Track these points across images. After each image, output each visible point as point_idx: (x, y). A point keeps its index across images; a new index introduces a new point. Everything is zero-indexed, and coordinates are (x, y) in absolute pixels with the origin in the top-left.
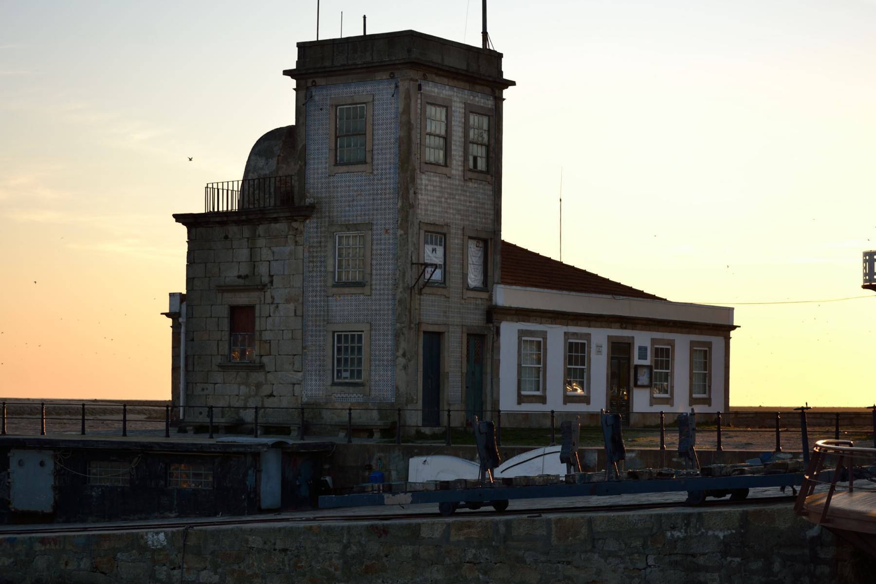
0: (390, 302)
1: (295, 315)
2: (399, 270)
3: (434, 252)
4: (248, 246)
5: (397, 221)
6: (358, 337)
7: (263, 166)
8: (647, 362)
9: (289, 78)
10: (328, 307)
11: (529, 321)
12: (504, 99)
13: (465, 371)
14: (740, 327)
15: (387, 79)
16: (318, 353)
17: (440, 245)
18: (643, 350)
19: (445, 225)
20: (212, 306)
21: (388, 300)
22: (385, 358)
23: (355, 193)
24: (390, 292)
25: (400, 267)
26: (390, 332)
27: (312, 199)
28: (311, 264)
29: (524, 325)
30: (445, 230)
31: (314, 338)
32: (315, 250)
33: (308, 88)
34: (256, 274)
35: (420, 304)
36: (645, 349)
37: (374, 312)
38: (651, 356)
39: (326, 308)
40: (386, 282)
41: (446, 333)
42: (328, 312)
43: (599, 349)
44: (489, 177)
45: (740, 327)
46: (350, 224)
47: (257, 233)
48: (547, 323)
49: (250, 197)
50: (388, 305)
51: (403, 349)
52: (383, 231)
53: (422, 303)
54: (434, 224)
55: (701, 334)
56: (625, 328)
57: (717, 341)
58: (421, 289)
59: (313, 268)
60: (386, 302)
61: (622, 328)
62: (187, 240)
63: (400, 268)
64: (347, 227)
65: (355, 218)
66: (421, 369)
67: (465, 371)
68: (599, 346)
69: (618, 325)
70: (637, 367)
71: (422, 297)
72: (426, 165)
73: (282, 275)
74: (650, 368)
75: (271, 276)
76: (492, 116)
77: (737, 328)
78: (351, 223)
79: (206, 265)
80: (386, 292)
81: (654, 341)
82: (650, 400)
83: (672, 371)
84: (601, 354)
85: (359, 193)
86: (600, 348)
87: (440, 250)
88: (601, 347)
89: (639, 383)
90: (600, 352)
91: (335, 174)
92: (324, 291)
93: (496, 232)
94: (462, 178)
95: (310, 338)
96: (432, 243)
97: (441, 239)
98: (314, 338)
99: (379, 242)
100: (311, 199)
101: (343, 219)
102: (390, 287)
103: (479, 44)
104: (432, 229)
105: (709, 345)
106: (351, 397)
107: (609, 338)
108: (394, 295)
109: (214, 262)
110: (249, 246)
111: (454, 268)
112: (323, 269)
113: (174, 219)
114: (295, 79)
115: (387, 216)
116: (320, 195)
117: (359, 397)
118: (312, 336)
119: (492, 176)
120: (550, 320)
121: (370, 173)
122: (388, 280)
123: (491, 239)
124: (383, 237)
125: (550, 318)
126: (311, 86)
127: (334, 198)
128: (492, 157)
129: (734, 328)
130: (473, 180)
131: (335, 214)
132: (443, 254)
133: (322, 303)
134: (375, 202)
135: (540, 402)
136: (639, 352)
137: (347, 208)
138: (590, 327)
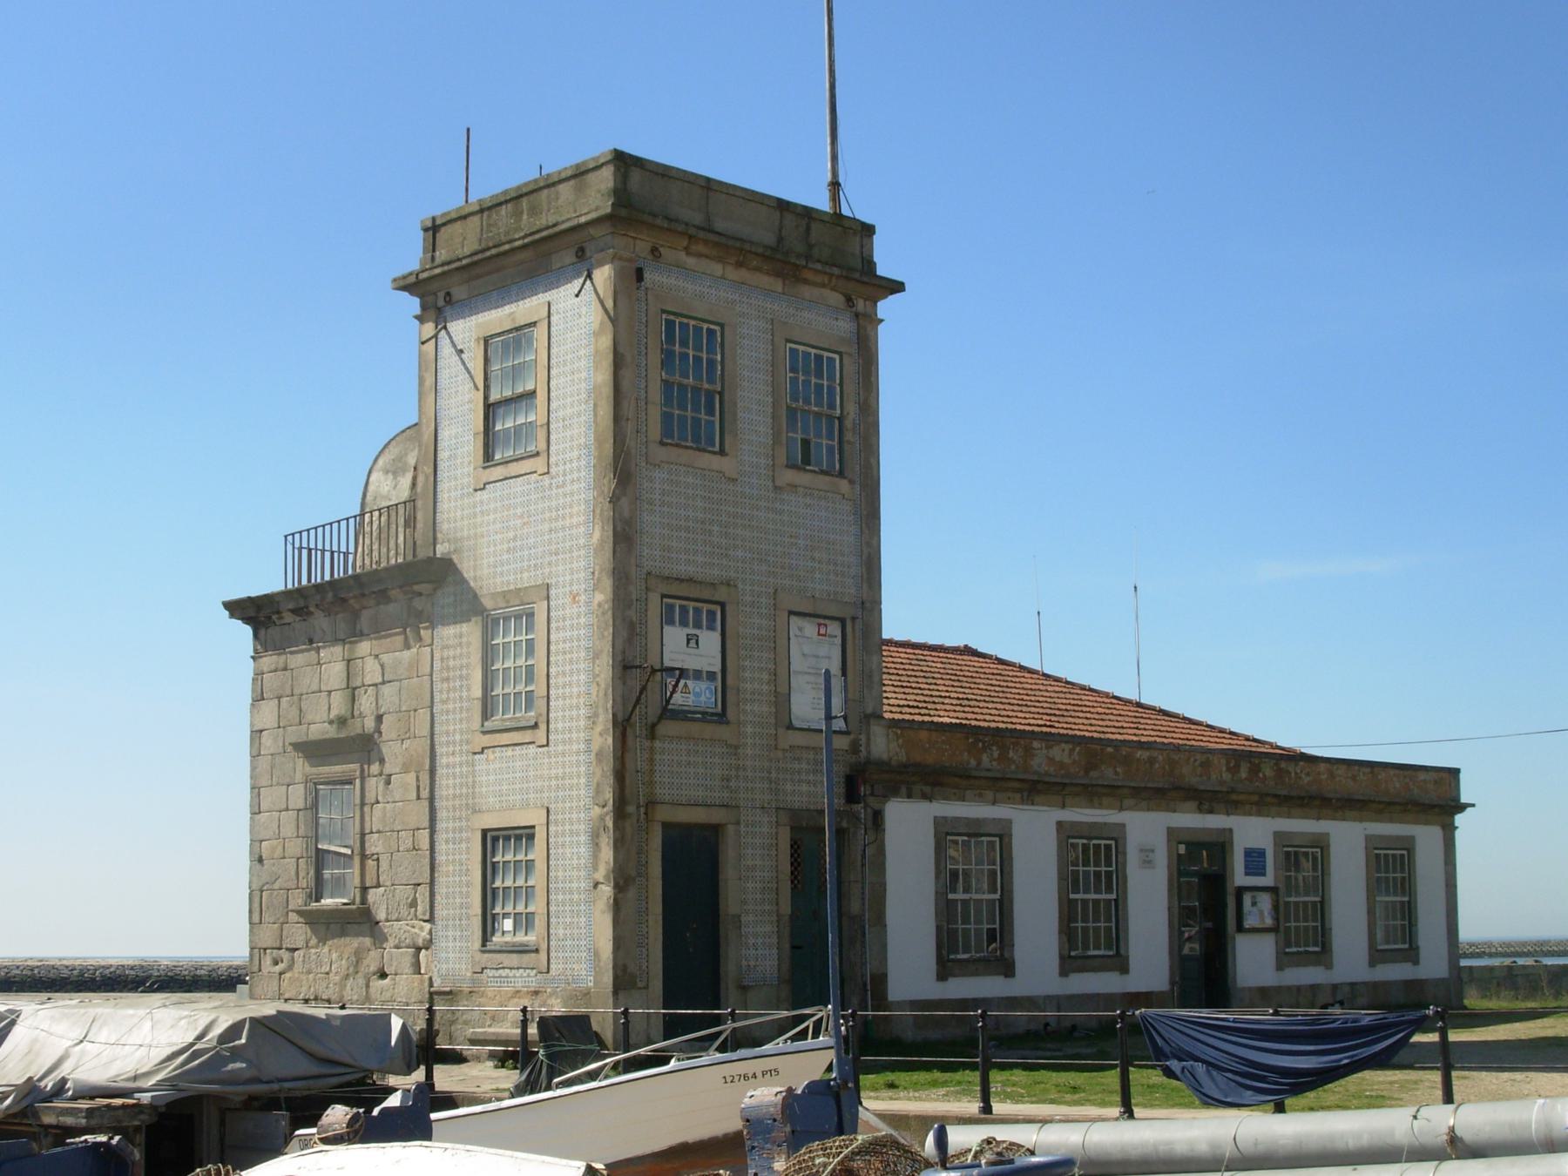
0: (582, 758)
1: (418, 798)
2: (598, 684)
3: (693, 643)
4: (343, 657)
5: (593, 573)
6: (1089, 861)
7: (389, 491)
8: (1267, 880)
9: (406, 294)
10: (474, 776)
11: (963, 799)
12: (881, 321)
13: (789, 911)
14: (1473, 805)
15: (573, 264)
16: (457, 879)
17: (711, 628)
18: (1255, 860)
19: (722, 583)
20: (288, 786)
21: (578, 753)
22: (575, 885)
23: (519, 522)
24: (582, 735)
25: (598, 675)
26: (582, 827)
27: (446, 545)
28: (445, 685)
29: (1077, 813)
30: (721, 594)
31: (451, 846)
32: (451, 653)
33: (439, 310)
34: (356, 713)
35: (652, 760)
36: (1261, 853)
37: (554, 783)
38: (1276, 869)
39: (470, 780)
40: (574, 713)
41: (731, 829)
42: (474, 787)
43: (1147, 856)
44: (844, 485)
45: (1473, 805)
46: (510, 591)
47: (358, 627)
48: (1009, 800)
49: (366, 557)
50: (578, 763)
51: (606, 862)
52: (568, 600)
53: (658, 757)
54: (690, 580)
55: (1391, 821)
56: (1211, 812)
57: (1426, 836)
58: (654, 726)
59: (448, 692)
60: (574, 758)
61: (1200, 811)
62: (253, 654)
63: (598, 679)
64: (504, 597)
65: (519, 576)
66: (657, 908)
67: (786, 909)
68: (1146, 851)
69: (1193, 805)
70: (1240, 891)
71: (657, 744)
72: (664, 448)
73: (397, 712)
74: (1273, 890)
75: (379, 719)
76: (850, 355)
77: (1469, 809)
78: (512, 587)
79: (279, 701)
80: (574, 735)
81: (1278, 836)
82: (1277, 958)
83: (1326, 897)
84: (1154, 868)
85: (526, 520)
86: (1151, 854)
87: (710, 641)
88: (1153, 851)
89: (1248, 923)
90: (1150, 862)
91: (485, 485)
92: (468, 742)
93: (868, 605)
94: (770, 484)
95: (444, 847)
96: (684, 623)
97: (711, 614)
98: (451, 846)
99: (561, 624)
100: (445, 544)
101: (498, 580)
102: (582, 723)
103: (822, 203)
104: (674, 589)
105: (1408, 845)
106: (515, 977)
107: (1173, 835)
108: (588, 741)
109: (292, 695)
110: (346, 657)
111: (752, 678)
112: (465, 694)
113: (227, 613)
114: (418, 296)
115: (575, 565)
116: (459, 535)
117: (529, 976)
118: (447, 842)
119: (851, 482)
120: (1018, 796)
121: (544, 474)
122: (578, 708)
123: (854, 619)
124: (568, 611)
125: (1019, 791)
126: (444, 306)
127: (483, 536)
128: (849, 442)
129: (1462, 808)
130: (799, 489)
131: (486, 571)
132: (720, 648)
133: (465, 769)
134: (553, 535)
135: (998, 974)
136: (1246, 861)
137: (505, 557)
138: (1121, 809)
